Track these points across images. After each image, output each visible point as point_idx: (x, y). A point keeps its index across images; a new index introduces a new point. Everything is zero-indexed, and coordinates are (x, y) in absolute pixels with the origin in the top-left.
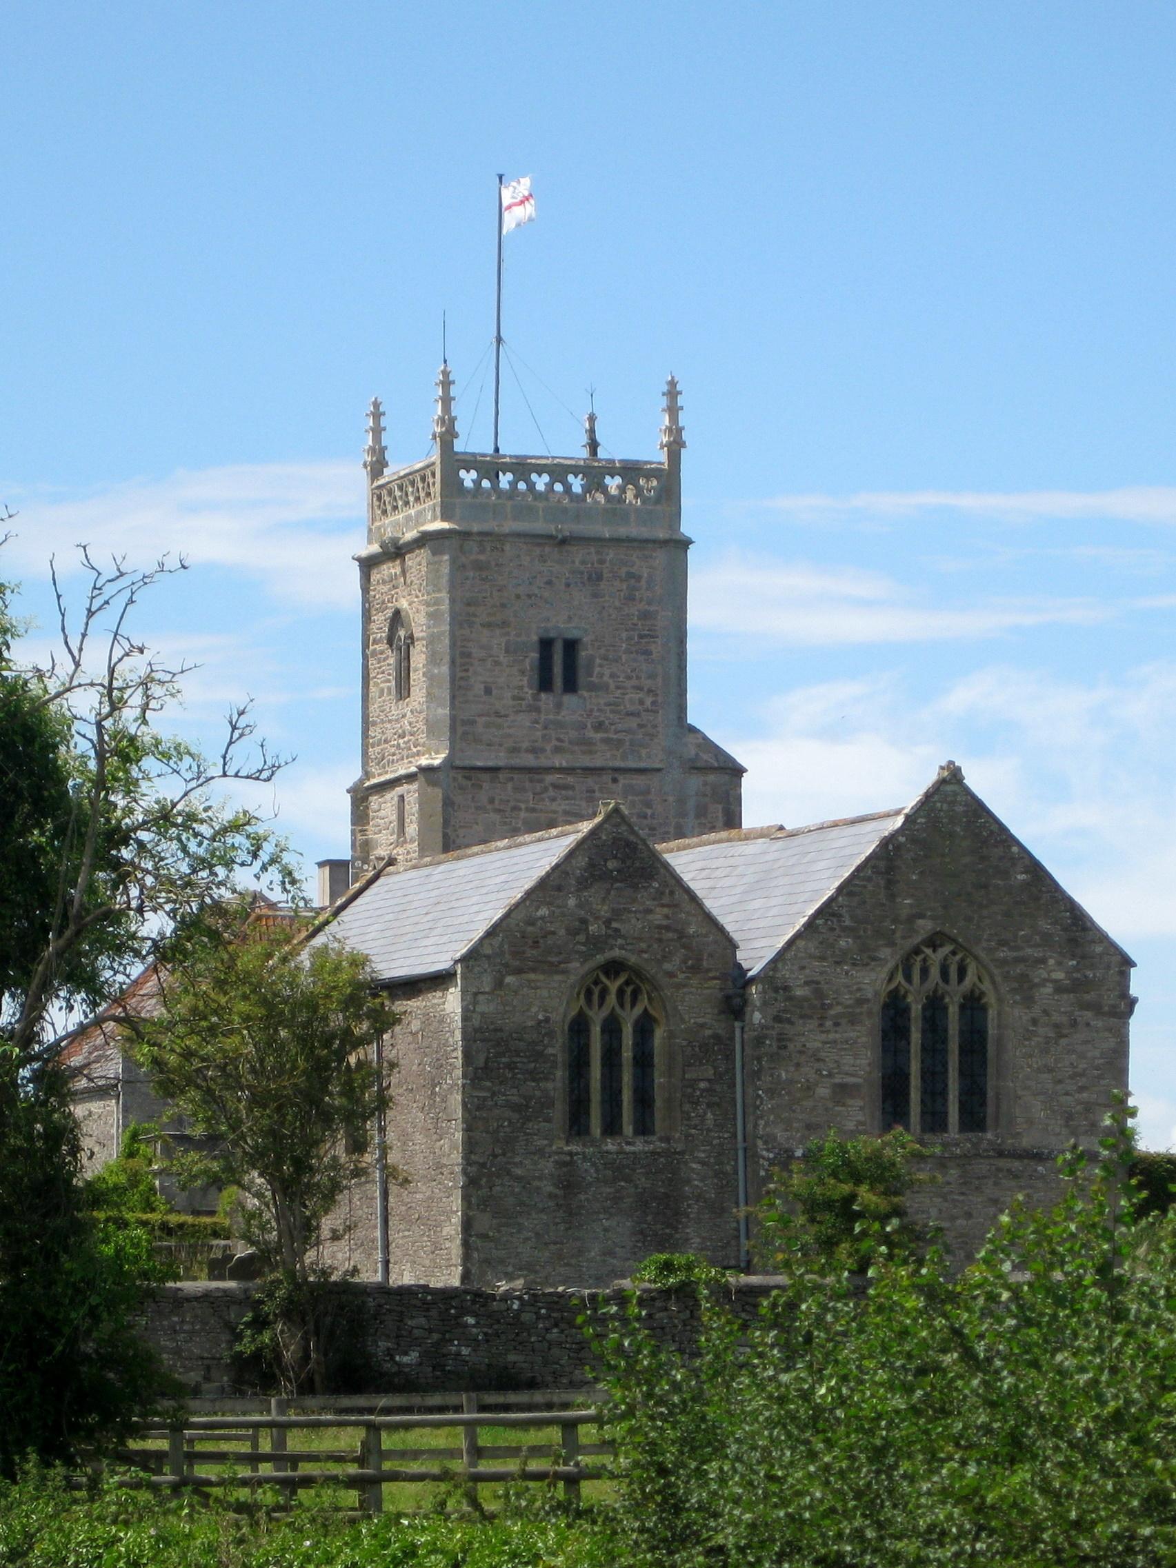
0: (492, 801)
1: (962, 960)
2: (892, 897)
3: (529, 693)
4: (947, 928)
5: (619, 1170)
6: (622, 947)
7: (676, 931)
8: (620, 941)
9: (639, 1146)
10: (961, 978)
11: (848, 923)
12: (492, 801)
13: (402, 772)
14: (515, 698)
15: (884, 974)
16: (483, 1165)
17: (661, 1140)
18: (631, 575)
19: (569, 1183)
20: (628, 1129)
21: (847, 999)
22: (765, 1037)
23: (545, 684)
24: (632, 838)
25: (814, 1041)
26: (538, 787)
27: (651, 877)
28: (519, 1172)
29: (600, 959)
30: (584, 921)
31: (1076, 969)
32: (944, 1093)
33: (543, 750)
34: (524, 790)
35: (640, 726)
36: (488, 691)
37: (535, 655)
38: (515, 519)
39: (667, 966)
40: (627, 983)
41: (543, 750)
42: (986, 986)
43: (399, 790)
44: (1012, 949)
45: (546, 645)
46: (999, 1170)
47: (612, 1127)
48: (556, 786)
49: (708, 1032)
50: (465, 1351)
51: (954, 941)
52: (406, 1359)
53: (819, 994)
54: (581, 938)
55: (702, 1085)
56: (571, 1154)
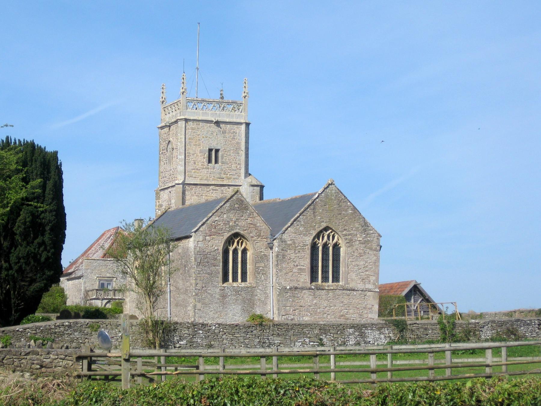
0: (195, 193)
1: (334, 234)
2: (315, 216)
3: (206, 163)
4: (330, 226)
5: (237, 291)
6: (239, 229)
7: (254, 225)
8: (238, 227)
9: (243, 284)
10: (333, 240)
11: (302, 223)
12: (195, 193)
13: (170, 185)
14: (202, 165)
15: (312, 238)
16: (199, 290)
17: (249, 283)
18: (234, 132)
19: (224, 296)
20: (240, 280)
21: (301, 244)
22: (279, 255)
23: (210, 161)
24: (242, 199)
25: (293, 256)
26: (208, 190)
27: (247, 209)
28: (209, 292)
29: (233, 232)
30: (229, 222)
31: (365, 237)
32: (328, 272)
33: (210, 180)
34: (204, 190)
35: (236, 173)
36: (195, 163)
37: (207, 153)
38: (202, 116)
39: (251, 235)
40: (240, 239)
41: (210, 180)
42: (340, 241)
43: (169, 190)
44: (348, 231)
45: (210, 150)
46: (344, 293)
47: (235, 279)
48: (213, 190)
49: (262, 254)
50: (199, 341)
51: (331, 229)
52: (182, 343)
53: (294, 243)
54: (228, 226)
55: (261, 268)
56: (224, 287)
